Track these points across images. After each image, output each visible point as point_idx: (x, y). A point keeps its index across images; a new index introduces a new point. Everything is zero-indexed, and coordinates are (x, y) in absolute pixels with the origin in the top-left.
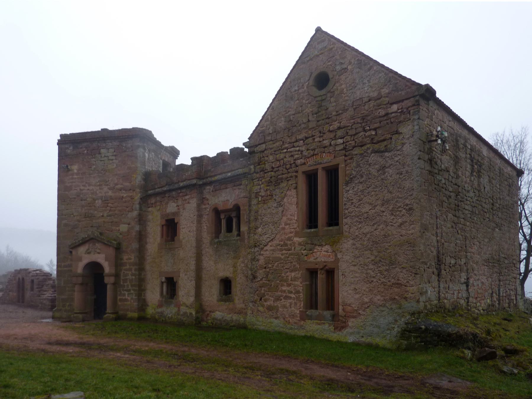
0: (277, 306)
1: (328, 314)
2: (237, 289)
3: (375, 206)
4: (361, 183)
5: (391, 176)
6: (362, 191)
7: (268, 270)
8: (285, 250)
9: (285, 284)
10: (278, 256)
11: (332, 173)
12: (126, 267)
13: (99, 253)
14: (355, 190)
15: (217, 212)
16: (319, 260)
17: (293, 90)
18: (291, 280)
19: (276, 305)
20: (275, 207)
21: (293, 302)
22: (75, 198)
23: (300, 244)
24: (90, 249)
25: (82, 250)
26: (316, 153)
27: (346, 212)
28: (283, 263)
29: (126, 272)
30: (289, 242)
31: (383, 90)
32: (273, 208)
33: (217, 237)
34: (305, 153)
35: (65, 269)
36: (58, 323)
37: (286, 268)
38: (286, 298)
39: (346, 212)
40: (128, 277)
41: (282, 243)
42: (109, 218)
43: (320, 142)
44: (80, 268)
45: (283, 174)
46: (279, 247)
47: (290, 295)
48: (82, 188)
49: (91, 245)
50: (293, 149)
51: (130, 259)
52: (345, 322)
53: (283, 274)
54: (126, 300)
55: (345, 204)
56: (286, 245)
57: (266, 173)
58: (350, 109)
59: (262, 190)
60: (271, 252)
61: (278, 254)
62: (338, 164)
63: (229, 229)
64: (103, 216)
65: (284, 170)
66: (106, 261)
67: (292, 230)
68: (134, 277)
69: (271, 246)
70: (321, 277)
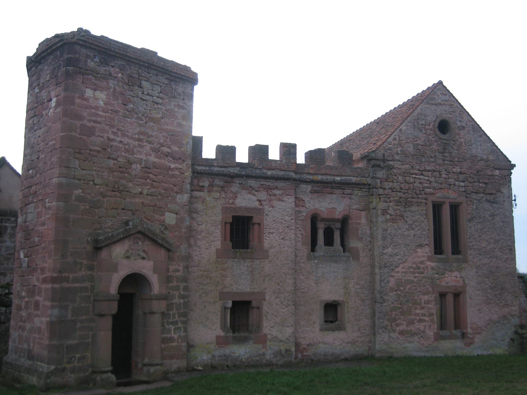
0: (411, 330)
1: (458, 333)
2: (348, 314)
3: (490, 243)
4: (480, 223)
5: (498, 223)
6: (481, 229)
7: (399, 293)
8: (418, 273)
9: (419, 307)
10: (410, 278)
11: (455, 208)
13: (143, 258)
14: (476, 227)
15: (314, 219)
16: (450, 284)
17: (420, 123)
18: (425, 304)
19: (409, 329)
20: (406, 229)
21: (428, 324)
22: (99, 152)
23: (432, 268)
26: (443, 187)
27: (471, 244)
28: (415, 286)
30: (422, 266)
31: (490, 156)
32: (404, 229)
33: (313, 249)
34: (435, 185)
35: (77, 285)
37: (420, 292)
38: (420, 321)
39: (471, 244)
40: (174, 301)
41: (415, 266)
42: (150, 198)
43: (446, 178)
45: (413, 198)
46: (411, 270)
47: (423, 318)
48: (112, 137)
50: (421, 177)
51: (178, 271)
52: (472, 339)
53: (416, 298)
54: (171, 339)
55: (469, 238)
56: (419, 268)
57: (393, 191)
58: (468, 161)
59: (391, 209)
60: (403, 274)
61: (410, 277)
62: (461, 203)
63: (329, 242)
64: (141, 193)
65: (414, 194)
66: (154, 273)
67: (425, 254)
68: (182, 301)
69: (402, 268)
70: (450, 299)
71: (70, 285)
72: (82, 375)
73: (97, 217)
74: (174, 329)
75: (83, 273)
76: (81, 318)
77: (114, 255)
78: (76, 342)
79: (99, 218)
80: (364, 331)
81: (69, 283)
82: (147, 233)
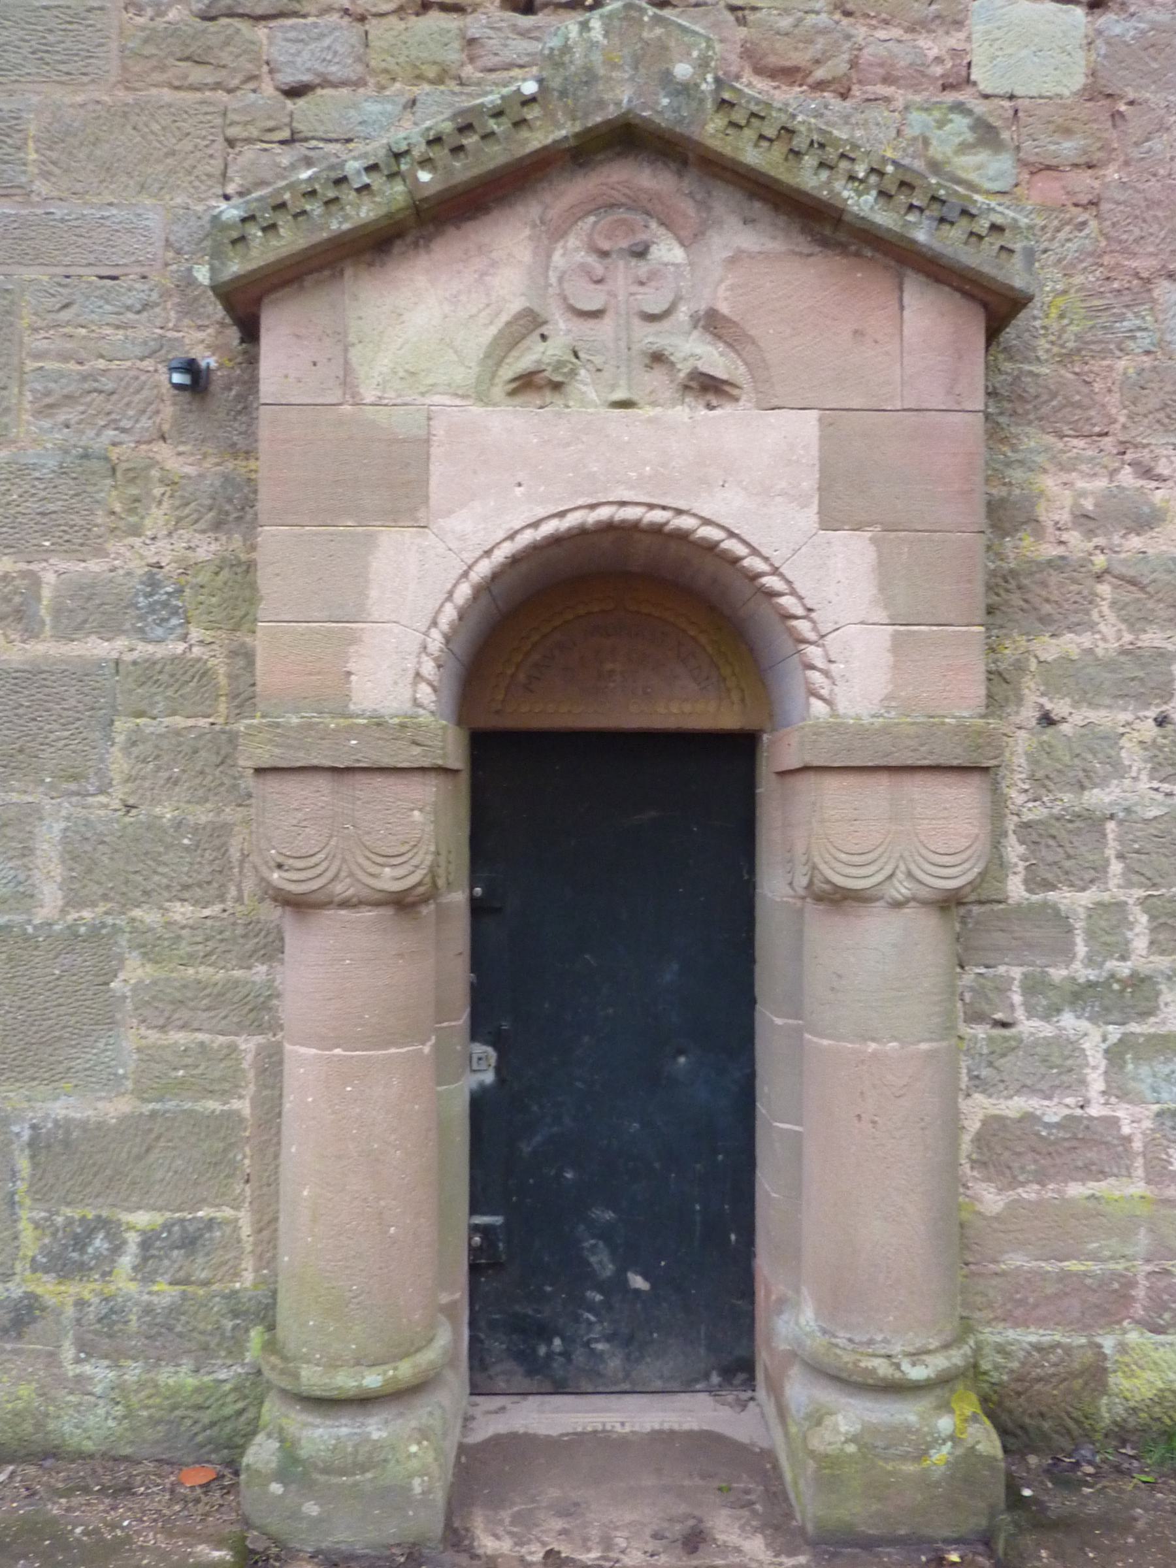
12: (1071, 644)
13: (708, 387)
25: (424, 324)
29: (1075, 717)
40: (1098, 798)
44: (390, 641)
49: (571, 253)
54: (1085, 1146)
66: (829, 521)
71: (44, 648)
72: (180, 1377)
74: (1115, 1055)
75: (164, 544)
76: (148, 916)
77: (376, 369)
78: (115, 1108)
79: (295, 92)
80: (226, 781)
81: (31, 633)
82: (711, 131)
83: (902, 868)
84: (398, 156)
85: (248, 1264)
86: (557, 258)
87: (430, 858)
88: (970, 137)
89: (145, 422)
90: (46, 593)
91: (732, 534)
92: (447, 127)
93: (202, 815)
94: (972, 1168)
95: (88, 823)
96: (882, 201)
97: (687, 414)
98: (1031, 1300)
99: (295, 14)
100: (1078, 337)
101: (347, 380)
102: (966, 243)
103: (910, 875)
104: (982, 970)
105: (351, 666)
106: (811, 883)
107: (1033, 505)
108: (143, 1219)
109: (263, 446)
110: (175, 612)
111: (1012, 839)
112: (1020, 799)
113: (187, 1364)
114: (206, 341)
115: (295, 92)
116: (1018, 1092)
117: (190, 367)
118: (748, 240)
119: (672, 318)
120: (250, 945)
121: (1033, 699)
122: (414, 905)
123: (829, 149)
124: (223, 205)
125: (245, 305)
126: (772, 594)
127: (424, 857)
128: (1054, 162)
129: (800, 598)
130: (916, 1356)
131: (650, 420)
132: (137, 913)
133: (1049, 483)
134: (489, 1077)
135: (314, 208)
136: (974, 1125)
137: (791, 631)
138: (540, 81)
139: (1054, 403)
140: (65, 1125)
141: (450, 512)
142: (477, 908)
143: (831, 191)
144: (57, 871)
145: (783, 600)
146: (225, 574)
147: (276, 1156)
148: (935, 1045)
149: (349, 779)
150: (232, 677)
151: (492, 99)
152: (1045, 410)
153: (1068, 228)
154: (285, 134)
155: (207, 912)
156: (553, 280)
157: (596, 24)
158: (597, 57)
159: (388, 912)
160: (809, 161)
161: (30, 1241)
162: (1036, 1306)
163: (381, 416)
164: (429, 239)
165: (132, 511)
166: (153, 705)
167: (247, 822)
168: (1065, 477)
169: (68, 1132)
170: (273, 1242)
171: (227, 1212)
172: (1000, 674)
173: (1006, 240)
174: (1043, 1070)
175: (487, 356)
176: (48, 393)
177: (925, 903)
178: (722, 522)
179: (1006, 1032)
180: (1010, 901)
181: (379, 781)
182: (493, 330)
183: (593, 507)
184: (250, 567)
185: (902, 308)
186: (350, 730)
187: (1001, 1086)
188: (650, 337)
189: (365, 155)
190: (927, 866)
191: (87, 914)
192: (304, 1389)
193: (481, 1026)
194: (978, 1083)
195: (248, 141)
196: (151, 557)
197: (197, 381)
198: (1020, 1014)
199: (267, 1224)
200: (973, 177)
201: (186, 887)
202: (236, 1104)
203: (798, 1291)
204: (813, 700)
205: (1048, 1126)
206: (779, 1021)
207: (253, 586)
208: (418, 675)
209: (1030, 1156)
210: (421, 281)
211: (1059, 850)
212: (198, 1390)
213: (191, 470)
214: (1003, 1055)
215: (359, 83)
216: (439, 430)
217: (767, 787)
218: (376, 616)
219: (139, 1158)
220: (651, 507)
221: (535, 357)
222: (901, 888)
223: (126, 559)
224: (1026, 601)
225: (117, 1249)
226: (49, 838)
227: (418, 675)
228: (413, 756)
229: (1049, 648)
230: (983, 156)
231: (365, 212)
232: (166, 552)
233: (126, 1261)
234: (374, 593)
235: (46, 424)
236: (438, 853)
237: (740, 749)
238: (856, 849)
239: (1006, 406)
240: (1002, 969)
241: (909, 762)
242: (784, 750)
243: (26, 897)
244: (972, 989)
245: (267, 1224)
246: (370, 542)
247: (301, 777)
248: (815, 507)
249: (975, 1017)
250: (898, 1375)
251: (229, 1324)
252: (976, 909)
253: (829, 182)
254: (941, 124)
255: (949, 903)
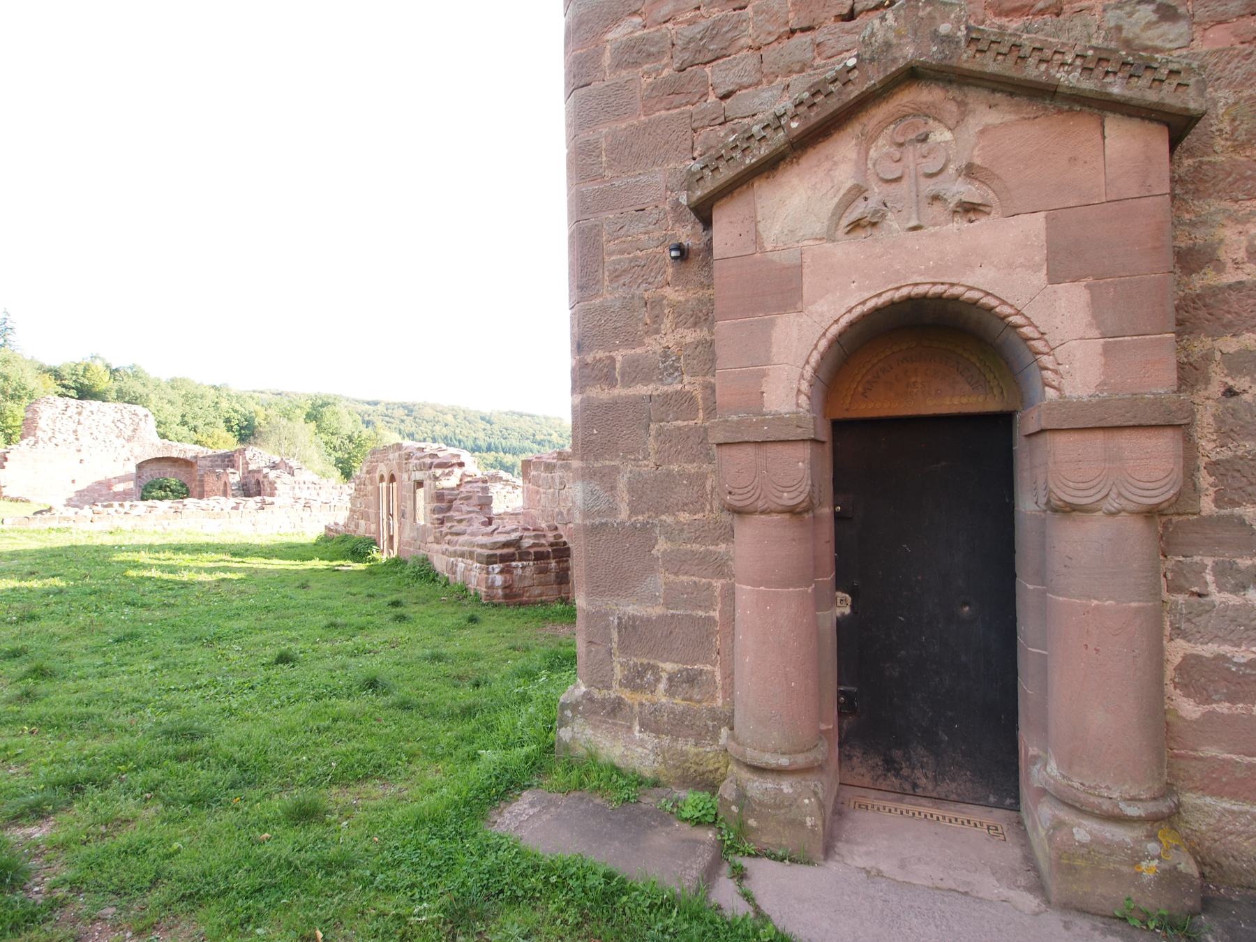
13: (969, 209)
24: (877, 192)
25: (795, 206)
35: (643, 390)
36: (841, 846)
44: (784, 369)
66: (1054, 278)
71: (619, 391)
73: (712, 98)
78: (655, 611)
79: (725, 97)
81: (612, 384)
82: (966, 59)
83: (1115, 490)
84: (779, 118)
85: (719, 694)
86: (872, 153)
87: (808, 488)
88: (1154, 17)
89: (659, 278)
90: (618, 366)
91: (988, 294)
92: (806, 95)
93: (692, 468)
94: (1175, 688)
95: (640, 474)
96: (1086, 73)
97: (959, 224)
98: (1224, 779)
99: (724, 56)
100: (1247, 132)
101: (757, 240)
102: (1150, 88)
103: (1120, 495)
104: (1181, 559)
105: (763, 389)
106: (1048, 502)
107: (1215, 250)
108: (669, 666)
109: (716, 281)
110: (676, 369)
111: (1203, 472)
112: (1210, 446)
113: (691, 741)
114: (687, 234)
115: (725, 97)
116: (1210, 640)
117: (679, 247)
118: (992, 118)
119: (945, 174)
120: (717, 534)
121: (1219, 377)
122: (800, 513)
123: (1046, 50)
124: (692, 162)
125: (704, 213)
126: (1016, 327)
127: (806, 487)
128: (1223, 18)
129: (1036, 327)
130: (1133, 800)
131: (932, 235)
132: (663, 517)
133: (1229, 233)
134: (847, 611)
135: (737, 154)
136: (1177, 660)
137: (1030, 348)
138: (857, 56)
139: (1230, 179)
140: (634, 618)
141: (814, 302)
142: (838, 517)
143: (1048, 75)
144: (626, 497)
145: (1023, 330)
146: (700, 348)
147: (733, 641)
148: (1142, 604)
149: (764, 447)
150: (704, 399)
151: (830, 74)
152: (1221, 185)
153: (1236, 60)
154: (722, 119)
155: (696, 517)
156: (870, 166)
157: (890, 16)
158: (891, 36)
159: (787, 516)
160: (1032, 61)
161: (618, 673)
162: (1227, 784)
163: (775, 257)
164: (798, 158)
165: (654, 322)
166: (668, 415)
167: (713, 471)
168: (1240, 228)
169: (634, 622)
170: (732, 684)
171: (709, 668)
172: (1191, 364)
173: (1183, 78)
174: (1232, 627)
175: (833, 215)
176: (616, 270)
177: (1132, 513)
178: (981, 287)
179: (1202, 600)
180: (1203, 514)
181: (780, 447)
182: (836, 200)
183: (898, 289)
184: (712, 343)
185: (1104, 138)
186: (764, 421)
187: (1198, 636)
188: (929, 187)
189: (762, 121)
190: (1133, 489)
191: (640, 518)
192: (748, 761)
193: (841, 583)
194: (1179, 632)
195: (703, 127)
196: (664, 343)
197: (683, 254)
198: (1212, 588)
199: (729, 676)
200: (1158, 43)
201: (686, 504)
202: (712, 613)
203: (1046, 752)
204: (1047, 389)
205: (1236, 664)
206: (1031, 587)
207: (714, 353)
208: (799, 390)
209: (1223, 683)
210: (795, 181)
211: (1244, 480)
212: (697, 755)
213: (682, 299)
214: (1199, 615)
215: (759, 83)
216: (807, 259)
217: (1020, 444)
218: (776, 361)
219: (667, 637)
220: (934, 284)
221: (861, 210)
222: (1113, 504)
223: (653, 346)
224: (1211, 314)
225: (658, 680)
226: (622, 483)
227: (799, 390)
228: (799, 433)
229: (1230, 345)
230: (1165, 27)
231: (764, 151)
232: (670, 340)
233: (662, 686)
234: (774, 350)
235: (615, 285)
236: (813, 485)
237: (1002, 423)
238: (1080, 479)
239: (1185, 188)
240: (1197, 559)
241: (1118, 423)
242: (1029, 422)
243: (613, 510)
244: (1172, 571)
245: (729, 676)
246: (772, 323)
247: (739, 447)
248: (1045, 271)
249: (1174, 588)
250: (1116, 811)
251: (710, 723)
252: (1175, 519)
253: (1047, 69)
254: (1130, 15)
255: (1151, 514)
